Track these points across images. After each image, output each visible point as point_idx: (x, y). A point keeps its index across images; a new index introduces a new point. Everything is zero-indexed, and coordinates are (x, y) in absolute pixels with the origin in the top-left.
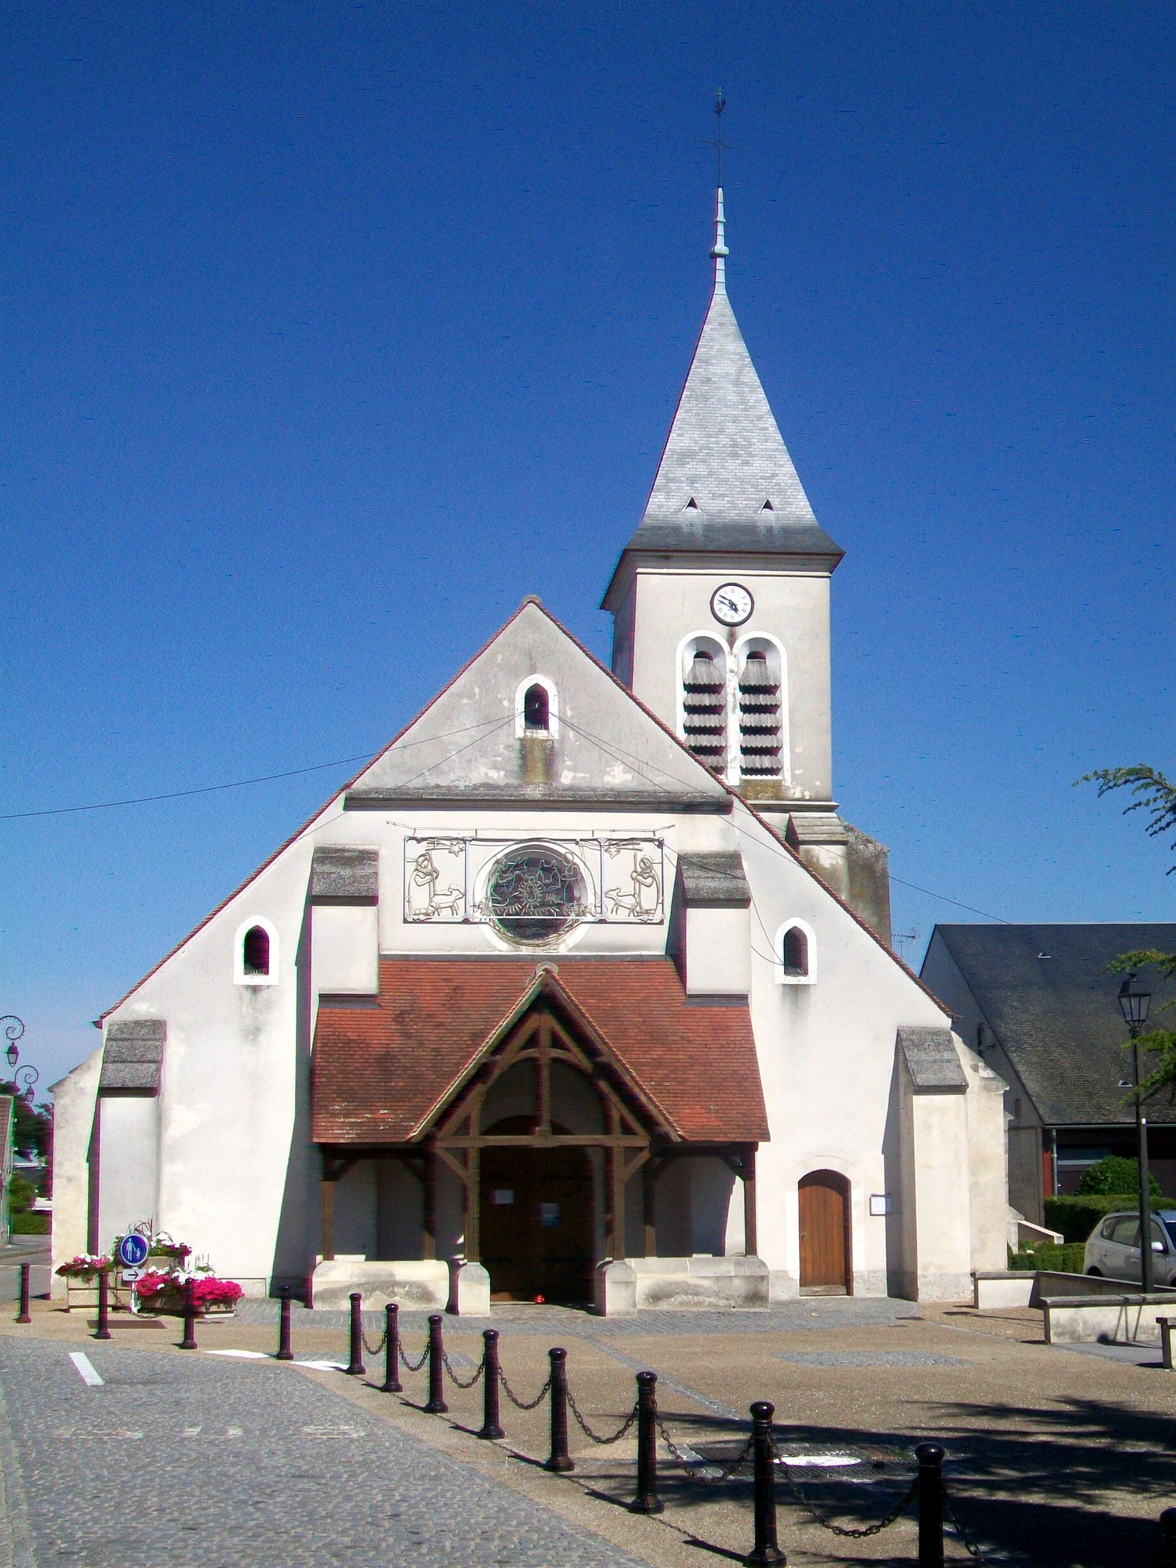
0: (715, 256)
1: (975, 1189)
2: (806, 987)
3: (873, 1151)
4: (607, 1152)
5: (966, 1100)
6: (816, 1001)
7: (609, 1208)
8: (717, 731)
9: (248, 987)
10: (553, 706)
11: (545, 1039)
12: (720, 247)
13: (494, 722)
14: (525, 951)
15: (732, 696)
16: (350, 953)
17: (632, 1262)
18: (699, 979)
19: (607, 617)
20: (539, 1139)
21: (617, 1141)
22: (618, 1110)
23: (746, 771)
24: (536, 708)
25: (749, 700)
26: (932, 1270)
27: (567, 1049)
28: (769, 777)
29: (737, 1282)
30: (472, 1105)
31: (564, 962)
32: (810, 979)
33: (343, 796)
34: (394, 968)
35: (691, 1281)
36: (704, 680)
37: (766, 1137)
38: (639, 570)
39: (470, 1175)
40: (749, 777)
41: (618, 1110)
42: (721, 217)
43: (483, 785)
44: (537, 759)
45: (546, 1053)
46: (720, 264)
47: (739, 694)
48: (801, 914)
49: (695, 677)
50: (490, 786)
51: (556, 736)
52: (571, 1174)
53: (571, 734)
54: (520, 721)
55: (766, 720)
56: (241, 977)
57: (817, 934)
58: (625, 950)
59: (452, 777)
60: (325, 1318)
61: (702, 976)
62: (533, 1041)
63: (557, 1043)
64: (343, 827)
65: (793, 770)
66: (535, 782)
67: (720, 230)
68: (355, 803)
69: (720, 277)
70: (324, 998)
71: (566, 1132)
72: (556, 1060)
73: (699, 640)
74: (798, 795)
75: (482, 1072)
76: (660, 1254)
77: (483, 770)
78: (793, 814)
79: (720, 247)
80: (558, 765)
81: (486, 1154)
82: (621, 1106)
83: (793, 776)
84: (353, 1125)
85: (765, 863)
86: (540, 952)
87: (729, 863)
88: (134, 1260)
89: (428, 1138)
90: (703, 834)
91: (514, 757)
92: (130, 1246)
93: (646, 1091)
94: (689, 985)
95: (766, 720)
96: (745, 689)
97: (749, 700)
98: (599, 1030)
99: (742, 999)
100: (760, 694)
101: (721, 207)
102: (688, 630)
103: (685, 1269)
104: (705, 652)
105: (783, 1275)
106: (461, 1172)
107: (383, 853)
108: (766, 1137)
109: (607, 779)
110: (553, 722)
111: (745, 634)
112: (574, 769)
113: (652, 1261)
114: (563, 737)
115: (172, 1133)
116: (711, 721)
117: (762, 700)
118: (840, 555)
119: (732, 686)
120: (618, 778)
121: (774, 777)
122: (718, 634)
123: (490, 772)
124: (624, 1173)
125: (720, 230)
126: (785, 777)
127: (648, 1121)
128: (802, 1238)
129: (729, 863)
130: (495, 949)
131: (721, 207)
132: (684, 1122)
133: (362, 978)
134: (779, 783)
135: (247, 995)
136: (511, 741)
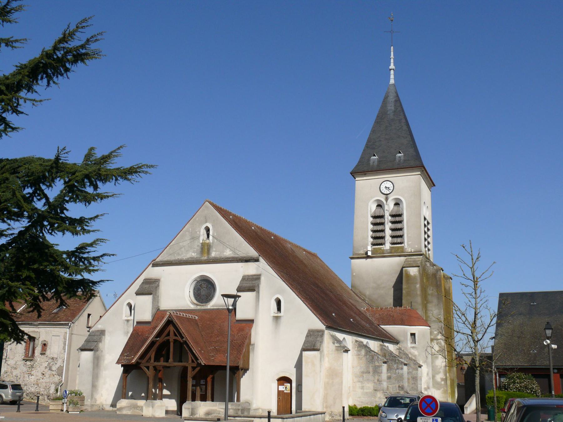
2: (280, 317)
6: (283, 321)
8: (383, 231)
11: (172, 333)
12: (392, 66)
15: (388, 218)
18: (240, 315)
28: (399, 245)
32: (281, 314)
35: (218, 410)
40: (375, 247)
42: (392, 56)
44: (206, 248)
46: (392, 72)
48: (279, 294)
51: (211, 241)
53: (215, 241)
55: (399, 226)
64: (153, 272)
65: (408, 242)
66: (205, 257)
67: (392, 61)
68: (155, 265)
73: (378, 200)
74: (409, 251)
75: (153, 343)
79: (392, 66)
80: (211, 251)
82: (154, 353)
83: (408, 244)
87: (257, 278)
90: (251, 269)
91: (199, 248)
95: (399, 226)
100: (397, 217)
101: (392, 53)
102: (372, 198)
103: (216, 406)
107: (162, 280)
109: (225, 253)
111: (391, 197)
112: (216, 251)
114: (213, 241)
117: (398, 219)
119: (387, 215)
120: (228, 253)
121: (401, 245)
122: (382, 198)
123: (193, 254)
125: (392, 61)
126: (406, 245)
131: (392, 53)
135: (126, 322)
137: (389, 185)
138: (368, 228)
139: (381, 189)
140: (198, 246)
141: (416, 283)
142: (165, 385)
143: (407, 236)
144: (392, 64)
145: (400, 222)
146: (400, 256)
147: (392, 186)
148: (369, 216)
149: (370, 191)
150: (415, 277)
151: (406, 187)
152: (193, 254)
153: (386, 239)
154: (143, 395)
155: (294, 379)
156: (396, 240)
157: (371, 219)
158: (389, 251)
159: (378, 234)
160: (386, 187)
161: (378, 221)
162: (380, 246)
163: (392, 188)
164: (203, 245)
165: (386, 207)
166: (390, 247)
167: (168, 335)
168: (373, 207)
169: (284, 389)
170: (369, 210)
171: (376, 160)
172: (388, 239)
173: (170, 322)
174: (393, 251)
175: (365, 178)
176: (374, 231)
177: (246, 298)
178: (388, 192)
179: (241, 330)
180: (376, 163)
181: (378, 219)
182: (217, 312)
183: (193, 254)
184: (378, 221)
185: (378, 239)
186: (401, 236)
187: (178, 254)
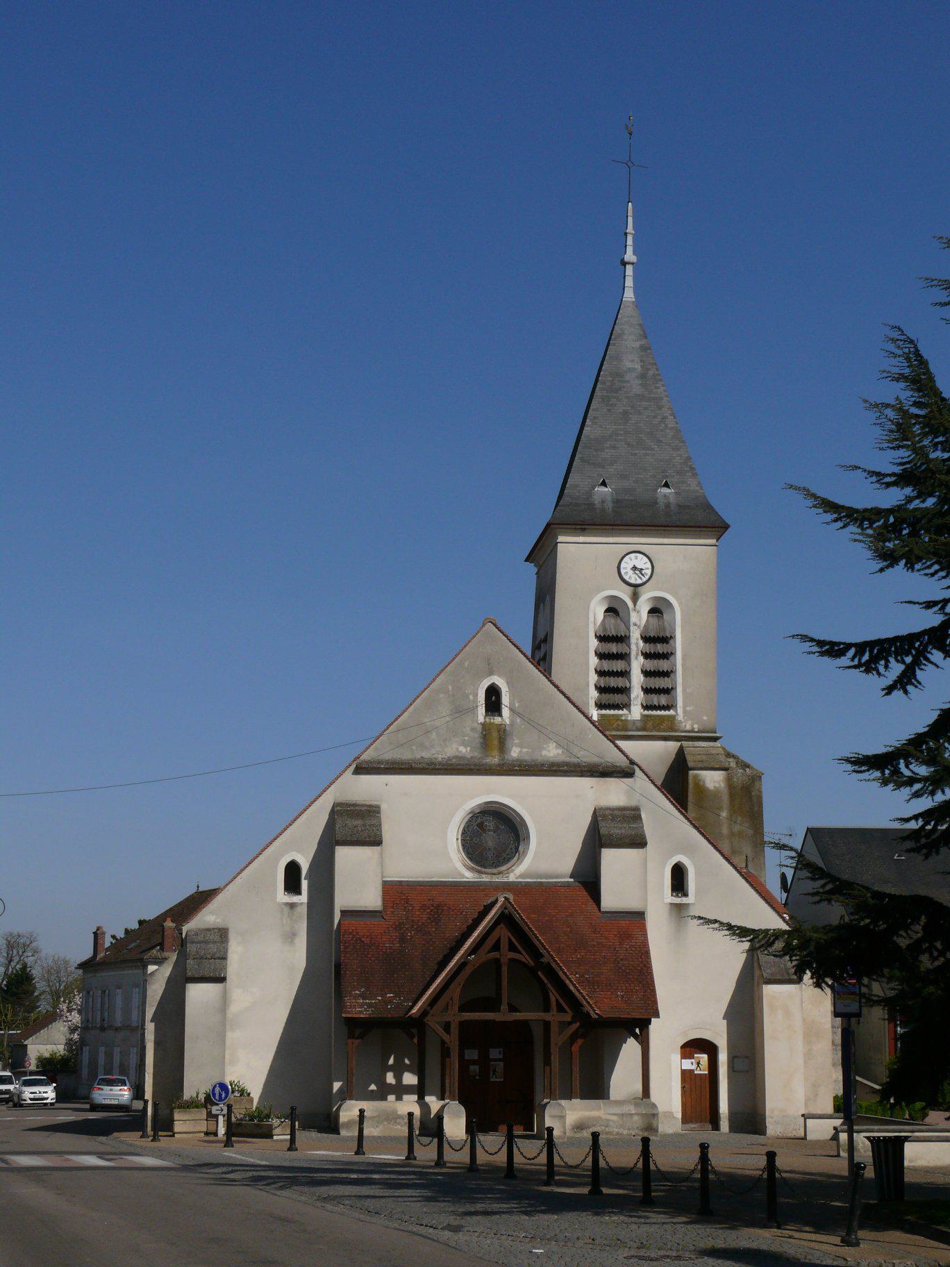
0: (624, 264)
1: (808, 1056)
2: (687, 905)
3: (724, 1023)
4: (547, 1025)
5: (801, 989)
7: (547, 1062)
9: (287, 904)
10: (505, 700)
11: (504, 945)
12: (630, 256)
13: (463, 711)
14: (486, 878)
15: (636, 644)
16: (360, 881)
17: (563, 1102)
18: (610, 900)
19: (532, 569)
20: (503, 1015)
21: (553, 1017)
22: (554, 996)
23: (646, 707)
24: (493, 700)
25: (650, 648)
26: (776, 1112)
27: (499, 940)
28: (663, 713)
29: (636, 1118)
30: (455, 991)
31: (518, 889)
32: (690, 899)
33: (354, 766)
34: (395, 892)
35: (605, 1117)
36: (613, 632)
37: (657, 1016)
38: (560, 539)
39: (453, 1040)
40: (650, 712)
41: (554, 996)
43: (456, 757)
44: (493, 738)
45: (506, 955)
46: (629, 270)
47: (641, 643)
49: (605, 629)
50: (462, 758)
51: (508, 722)
52: (519, 1042)
54: (481, 710)
55: (663, 665)
56: (282, 897)
57: (695, 866)
58: (557, 877)
59: (433, 751)
60: (347, 1139)
61: (614, 896)
62: (496, 947)
63: (512, 948)
65: (684, 707)
68: (361, 770)
69: (629, 282)
70: (343, 913)
71: (516, 1010)
72: (512, 960)
74: (688, 727)
75: (462, 966)
76: (583, 1098)
77: (455, 746)
78: (685, 744)
80: (508, 743)
81: (462, 1024)
82: (459, 990)
83: (685, 712)
84: (370, 1005)
85: (659, 814)
86: (496, 879)
87: (632, 815)
88: (221, 1100)
89: (424, 1013)
90: (614, 794)
92: (217, 1089)
93: (573, 981)
94: (603, 904)
95: (663, 665)
96: (646, 639)
97: (650, 648)
98: (541, 938)
99: (640, 915)
100: (659, 644)
102: (599, 590)
103: (599, 1109)
104: (614, 610)
105: (670, 1115)
106: (445, 1037)
107: (384, 807)
108: (657, 1016)
109: (544, 753)
110: (506, 712)
112: (521, 746)
113: (576, 1102)
114: (512, 724)
115: (233, 1009)
116: (618, 666)
117: (660, 648)
118: (726, 527)
119: (635, 635)
120: (552, 752)
121: (667, 713)
122: (624, 594)
123: (461, 749)
124: (557, 1039)
126: (680, 712)
127: (575, 1003)
128: (683, 1088)
129: (632, 815)
130: (463, 876)
131: (630, 220)
132: (598, 1006)
133: (371, 899)
134: (673, 717)
135: (286, 909)
136: (475, 725)
137: (641, 562)
138: (587, 664)
139: (623, 572)
140: (473, 729)
141: (720, 808)
142: (407, 1061)
143: (684, 691)
144: (630, 250)
145: (666, 656)
146: (665, 739)
147: (649, 565)
148: (592, 635)
149: (593, 570)
150: (716, 794)
151: (675, 570)
152: (462, 749)
153: (633, 696)
154: (373, 1087)
155: (722, 1043)
156: (655, 699)
157: (594, 643)
158: (639, 724)
159: (614, 682)
160: (634, 568)
161: (614, 648)
162: (616, 712)
163: (649, 572)
164: (486, 729)
165: (634, 618)
166: (643, 716)
167: (496, 947)
168: (597, 612)
169: (694, 1067)
170: (591, 619)
171: (609, 498)
172: (637, 694)
173: (506, 918)
174: (650, 724)
175: (581, 539)
176: (601, 673)
177: (613, 861)
178: (639, 582)
179: (625, 936)
180: (609, 506)
181: (612, 644)
182: (539, 893)
183: (462, 749)
184: (614, 648)
185: (612, 692)
186: (667, 691)
187: (422, 746)
